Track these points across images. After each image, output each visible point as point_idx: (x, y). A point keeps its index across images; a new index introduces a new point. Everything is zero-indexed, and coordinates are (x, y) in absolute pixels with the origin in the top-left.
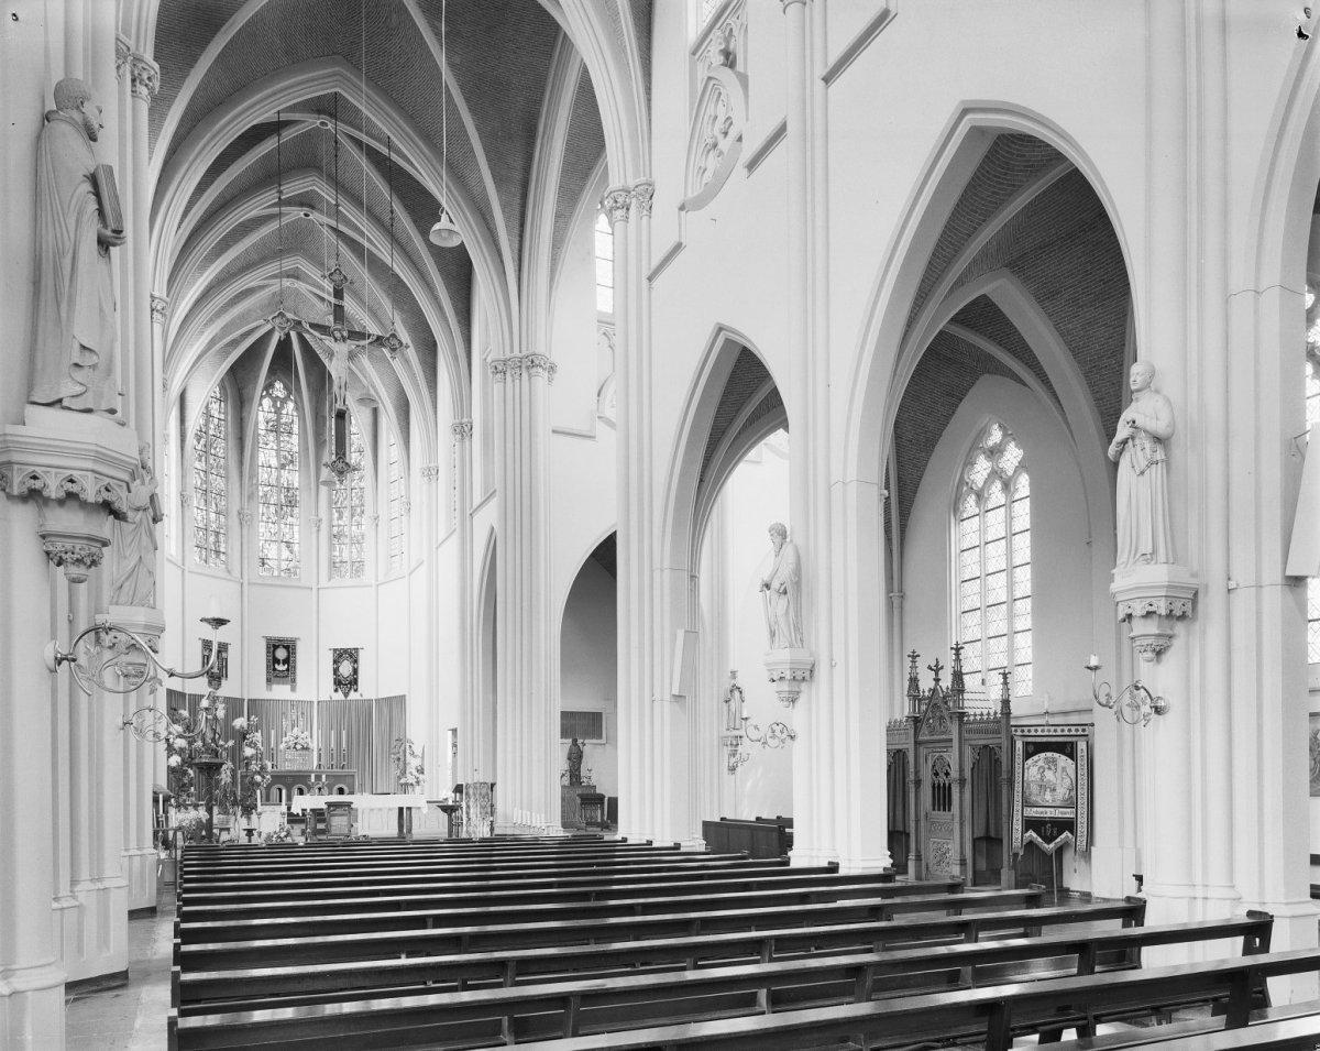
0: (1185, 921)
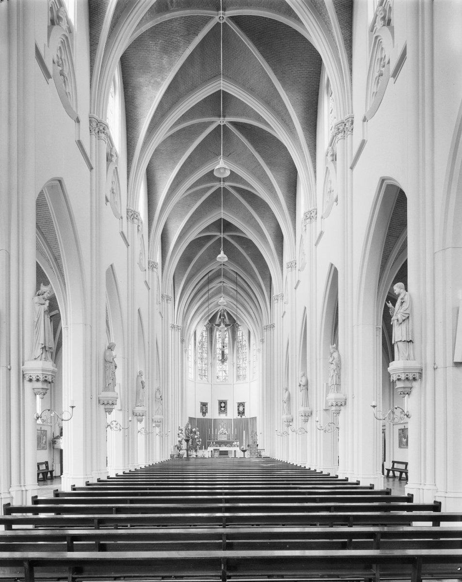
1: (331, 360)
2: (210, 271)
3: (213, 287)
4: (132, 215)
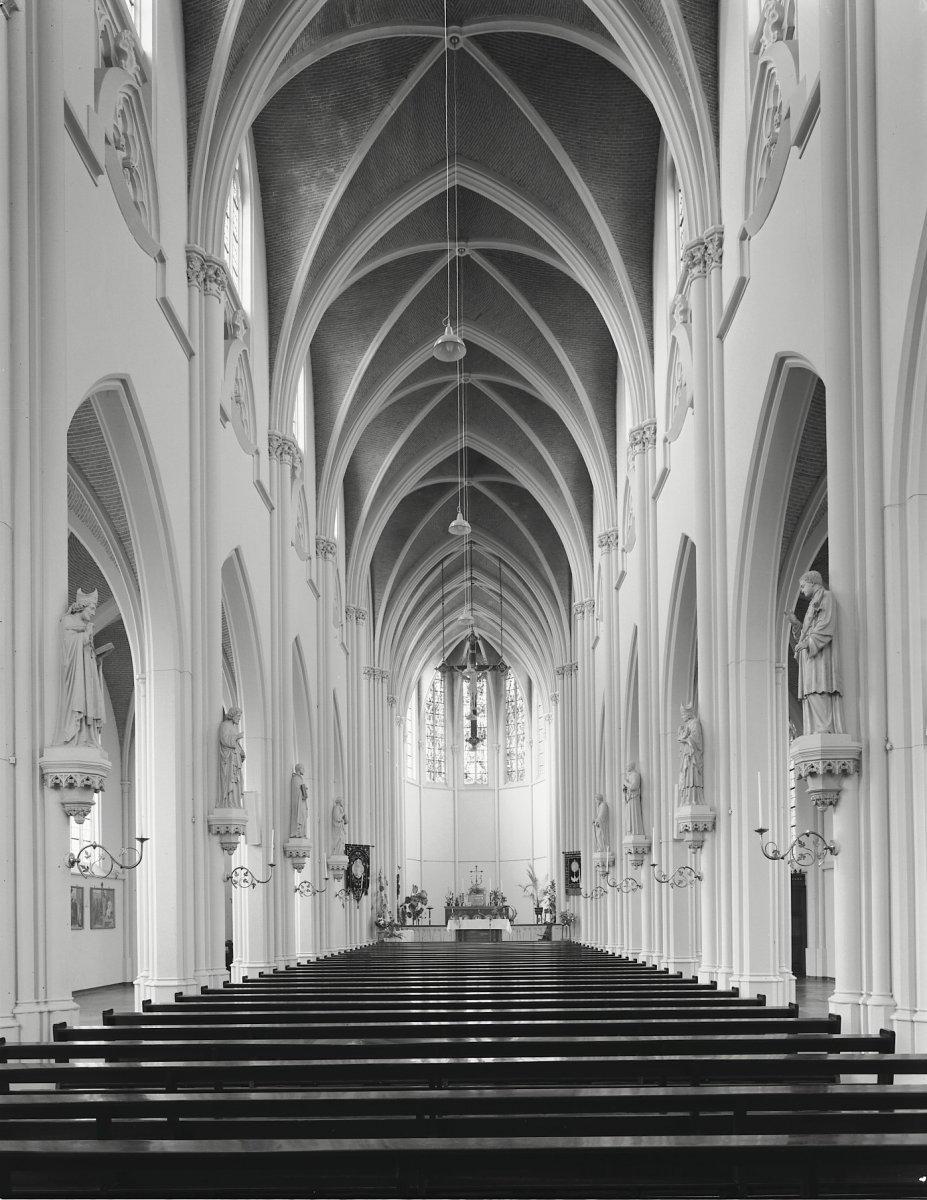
0: (907, 1053)
1: (681, 737)
2: (446, 558)
3: (456, 589)
4: (281, 446)
